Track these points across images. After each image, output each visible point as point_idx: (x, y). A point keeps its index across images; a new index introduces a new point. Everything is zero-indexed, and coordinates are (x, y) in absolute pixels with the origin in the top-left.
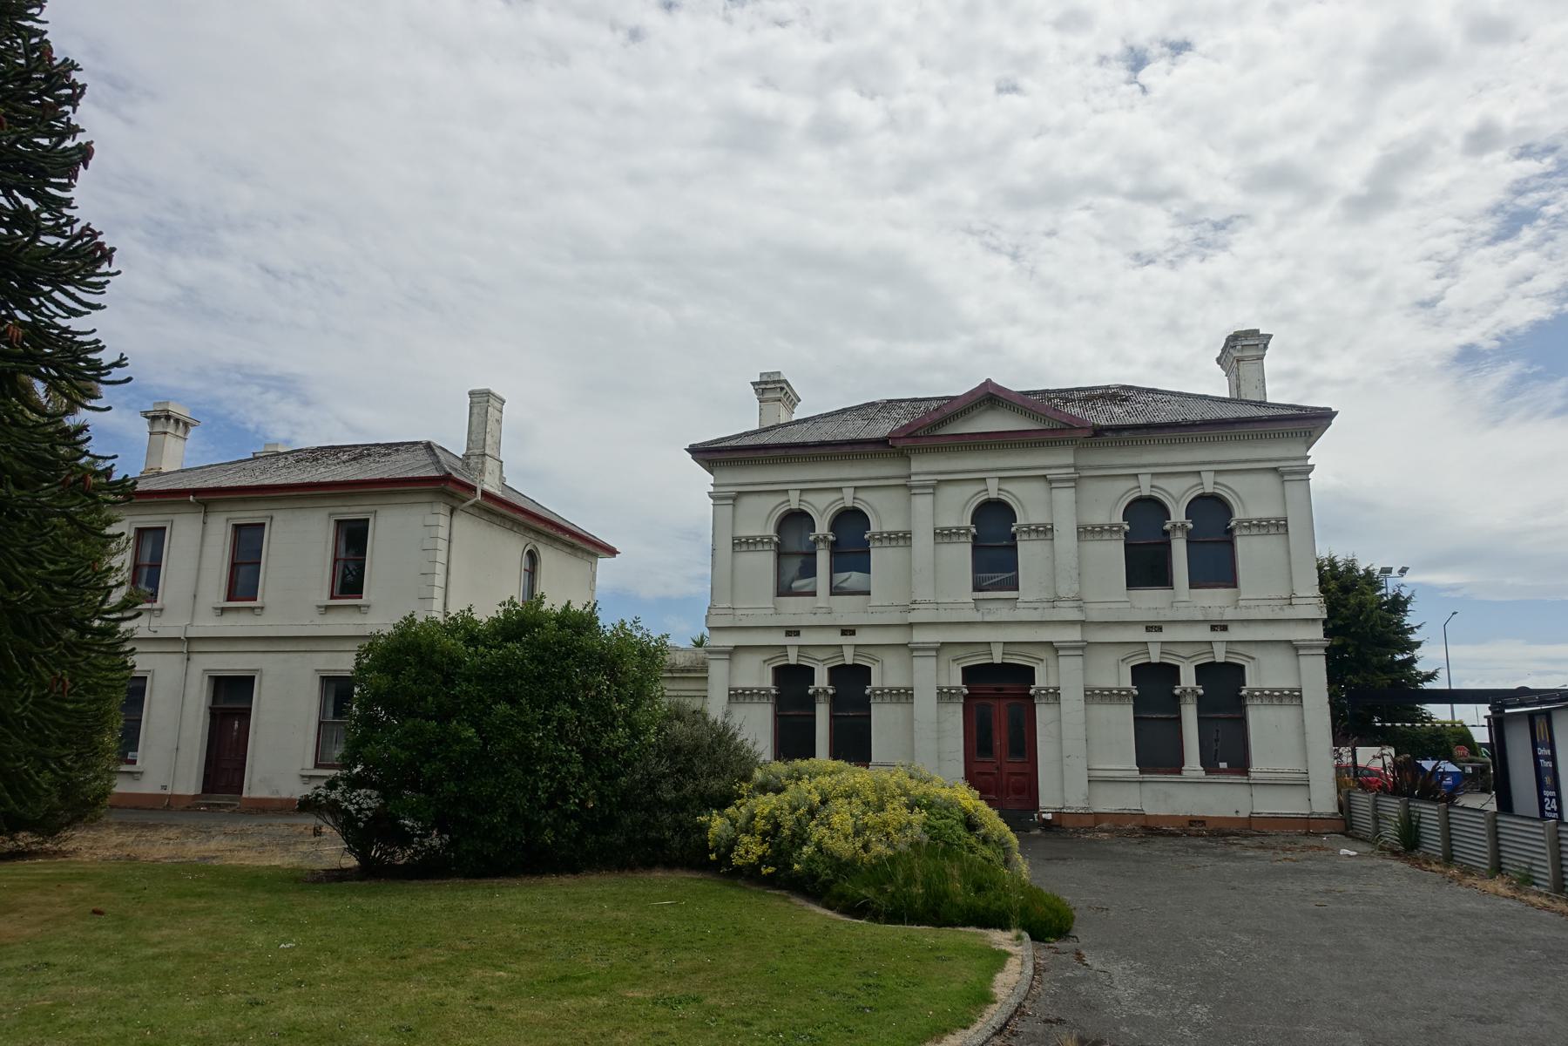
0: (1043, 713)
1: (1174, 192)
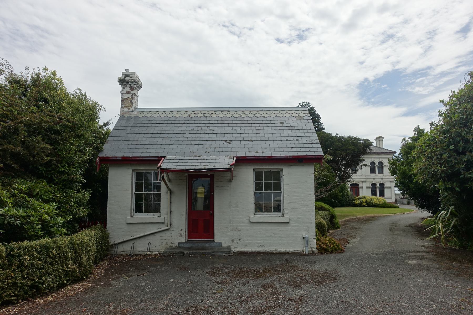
0: (360, 190)
1: (292, 16)
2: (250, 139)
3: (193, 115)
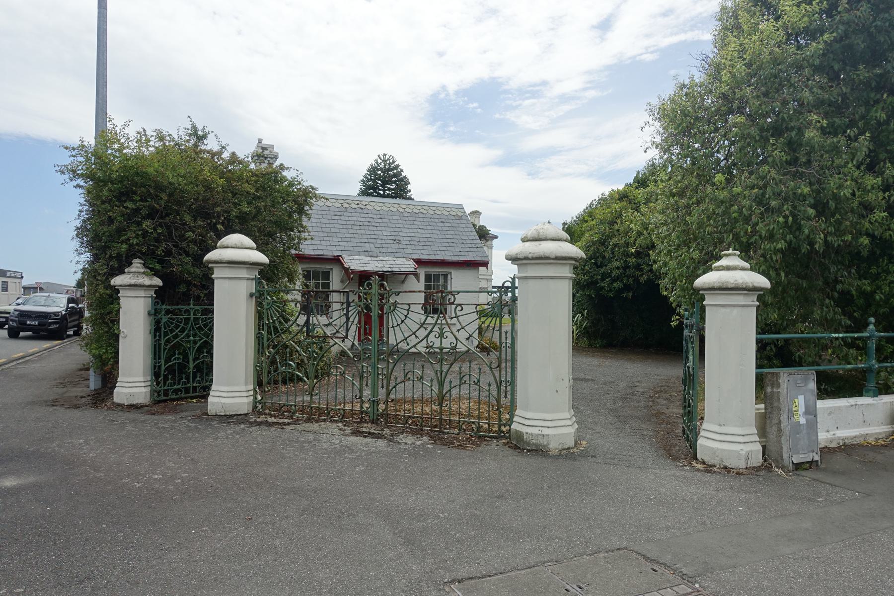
2: (418, 239)
3: (346, 205)
